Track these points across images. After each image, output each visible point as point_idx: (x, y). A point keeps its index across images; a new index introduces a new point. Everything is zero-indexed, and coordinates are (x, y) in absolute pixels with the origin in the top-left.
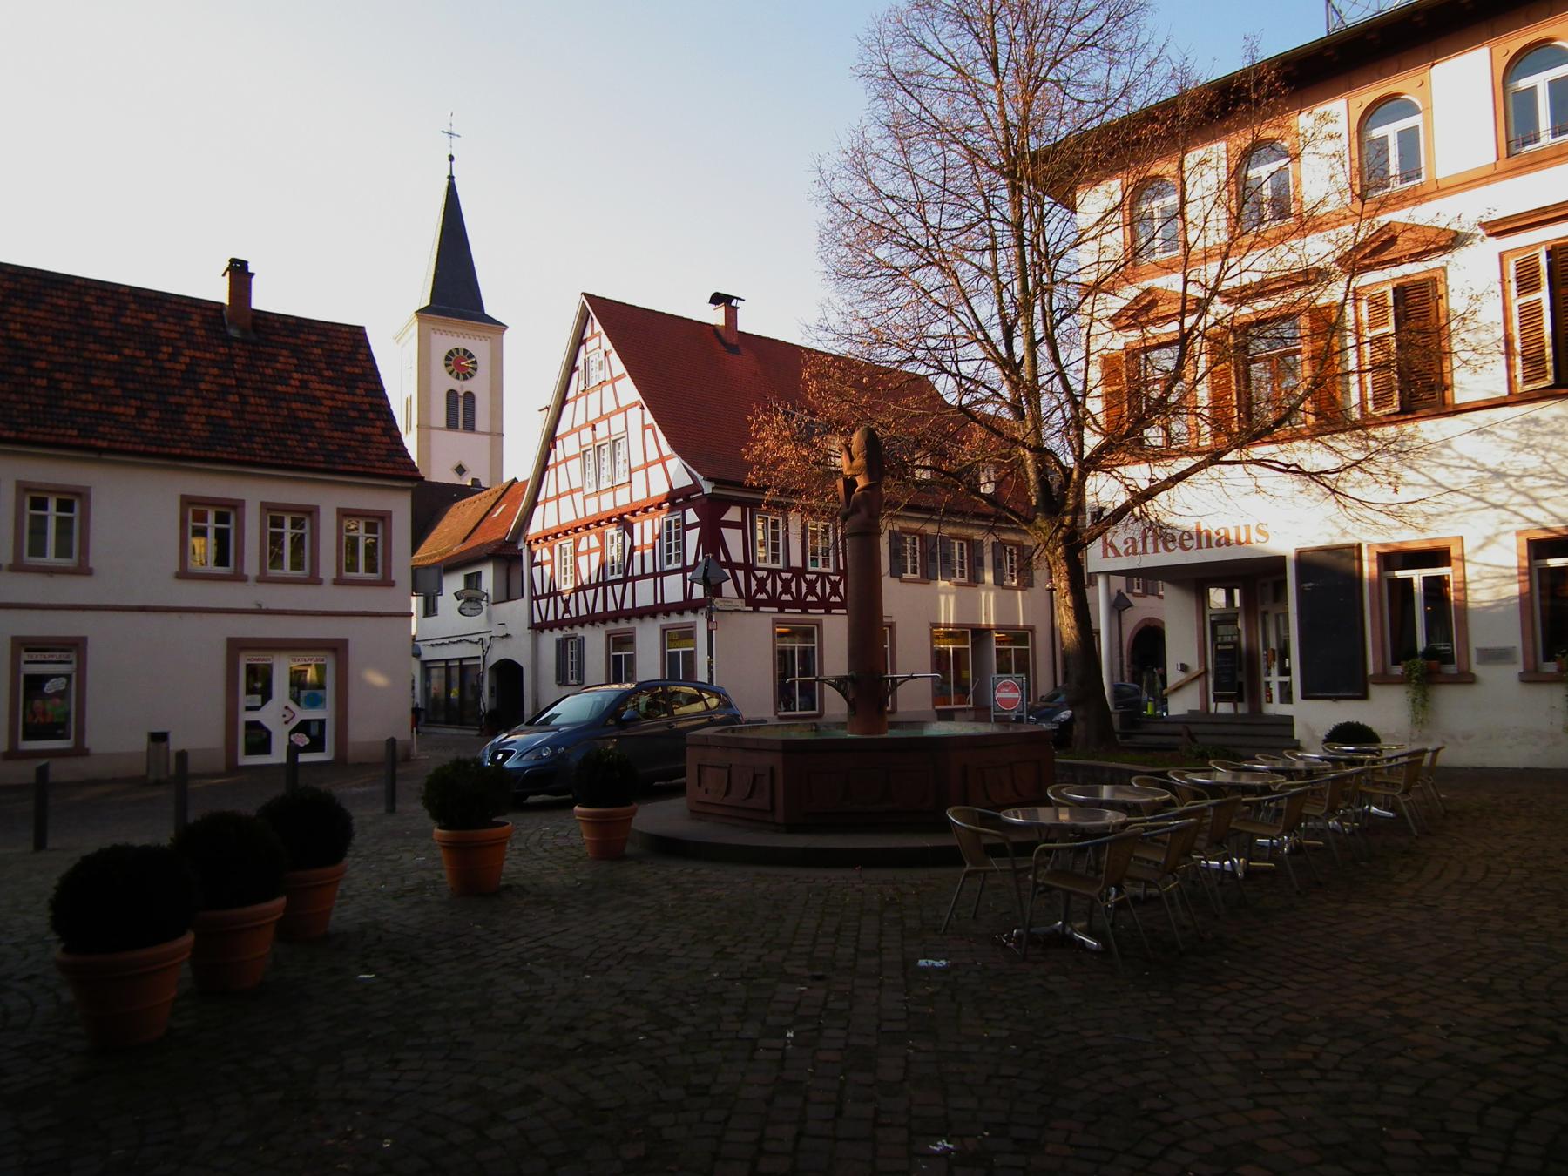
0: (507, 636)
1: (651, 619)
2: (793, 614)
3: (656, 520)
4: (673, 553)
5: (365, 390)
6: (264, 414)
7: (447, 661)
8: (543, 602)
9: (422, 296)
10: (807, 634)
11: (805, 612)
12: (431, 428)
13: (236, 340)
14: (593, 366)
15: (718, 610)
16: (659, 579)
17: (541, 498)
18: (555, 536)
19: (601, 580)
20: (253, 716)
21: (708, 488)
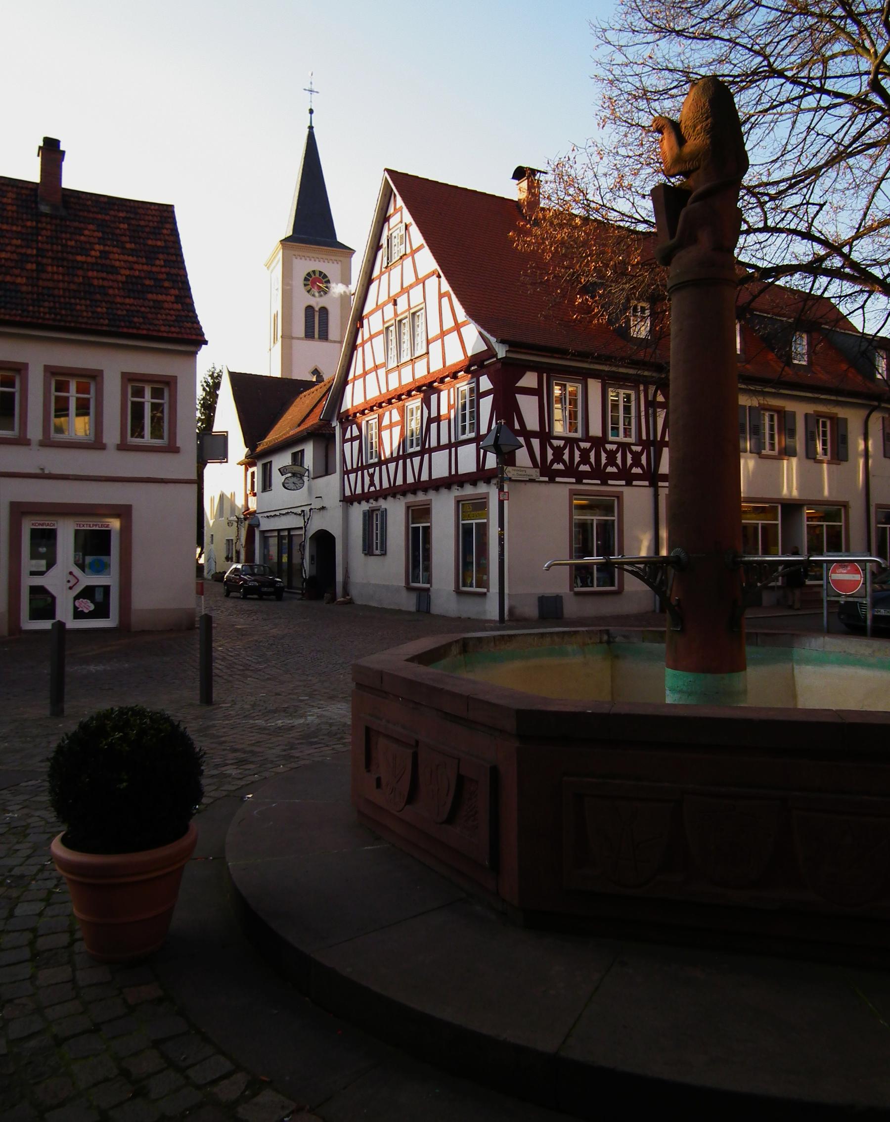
0: (323, 508)
1: (434, 492)
2: (592, 485)
3: (452, 390)
4: (467, 423)
5: (165, 261)
6: (59, 281)
7: (279, 531)
8: (352, 476)
9: (287, 230)
10: (608, 509)
11: (604, 483)
12: (293, 338)
13: (46, 215)
14: (395, 241)
15: (510, 480)
16: (453, 449)
17: (351, 376)
18: (363, 413)
19: (401, 453)
20: (37, 581)
21: (501, 351)
